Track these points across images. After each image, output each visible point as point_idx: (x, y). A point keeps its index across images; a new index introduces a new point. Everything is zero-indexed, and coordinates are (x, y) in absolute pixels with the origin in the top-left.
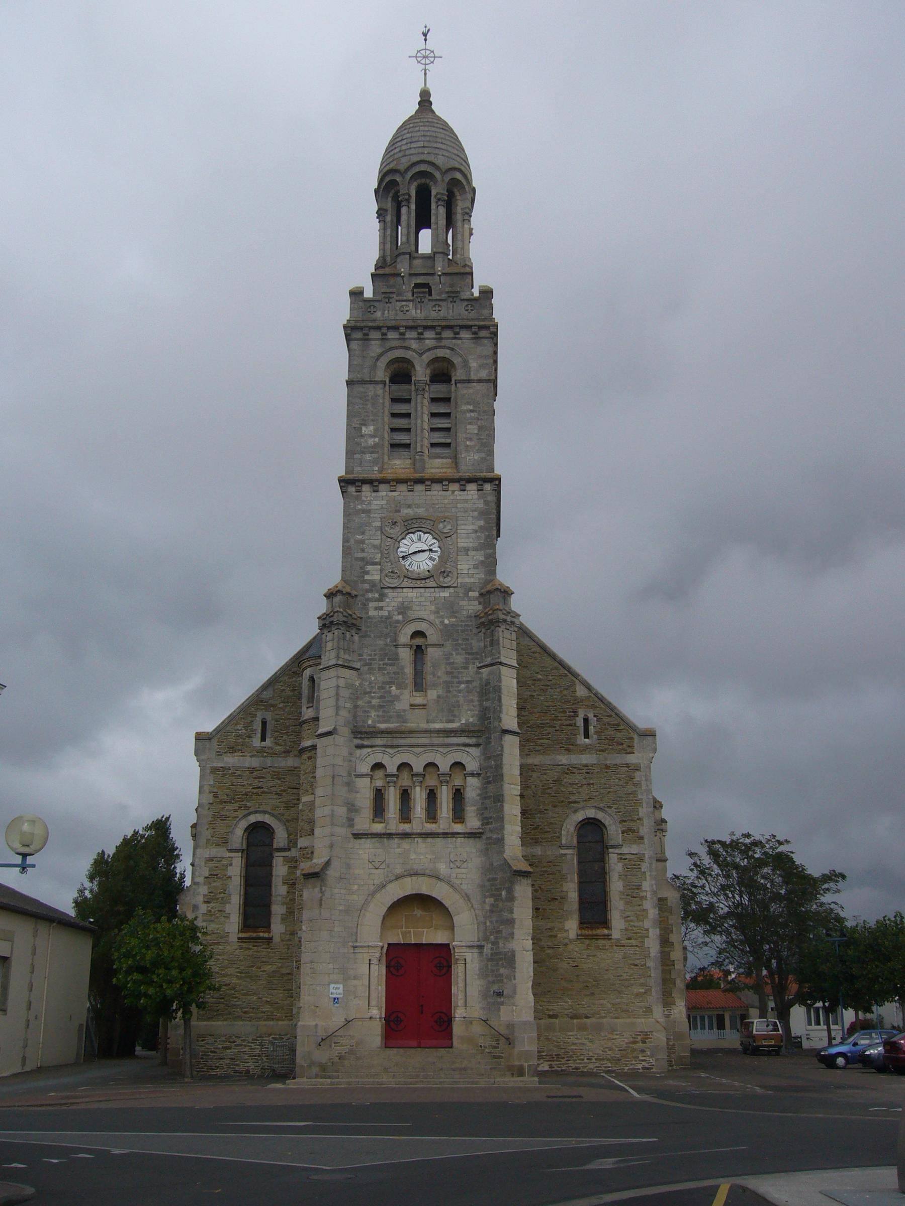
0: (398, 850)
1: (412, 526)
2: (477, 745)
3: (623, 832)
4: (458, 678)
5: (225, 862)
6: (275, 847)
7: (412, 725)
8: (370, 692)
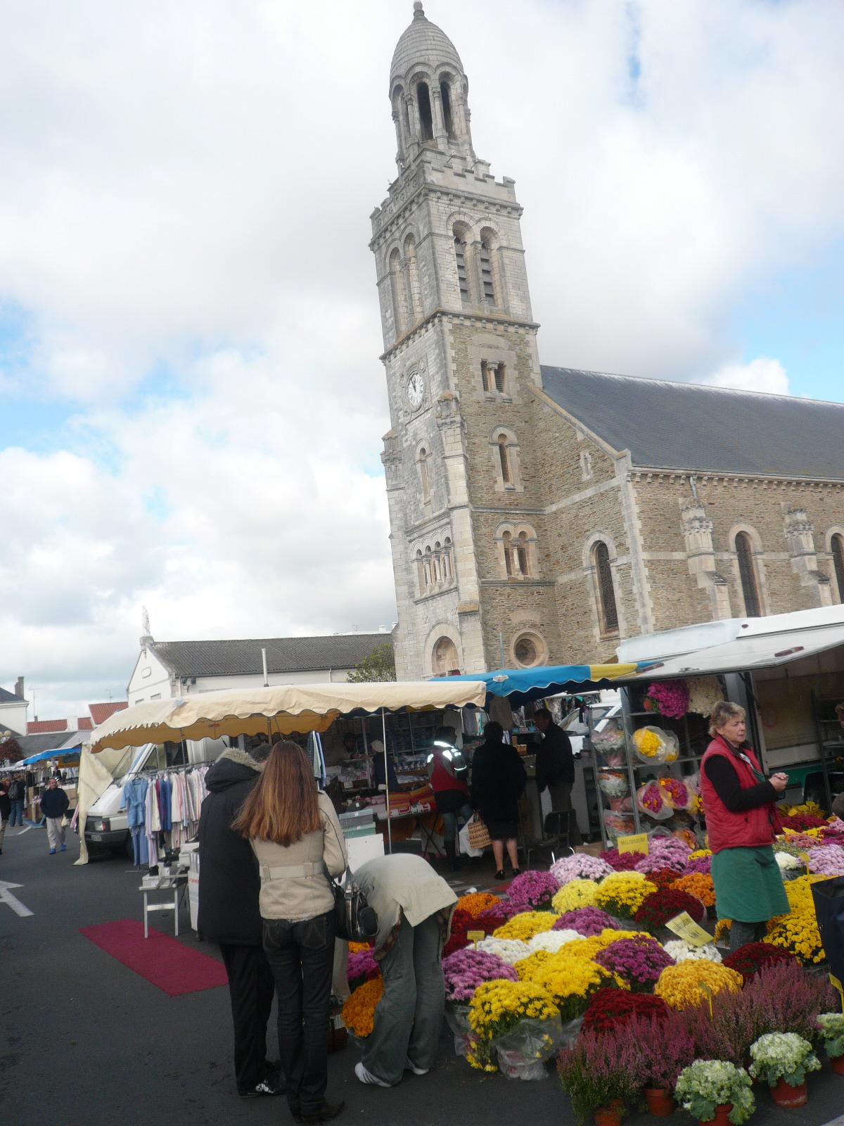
3: (616, 547)
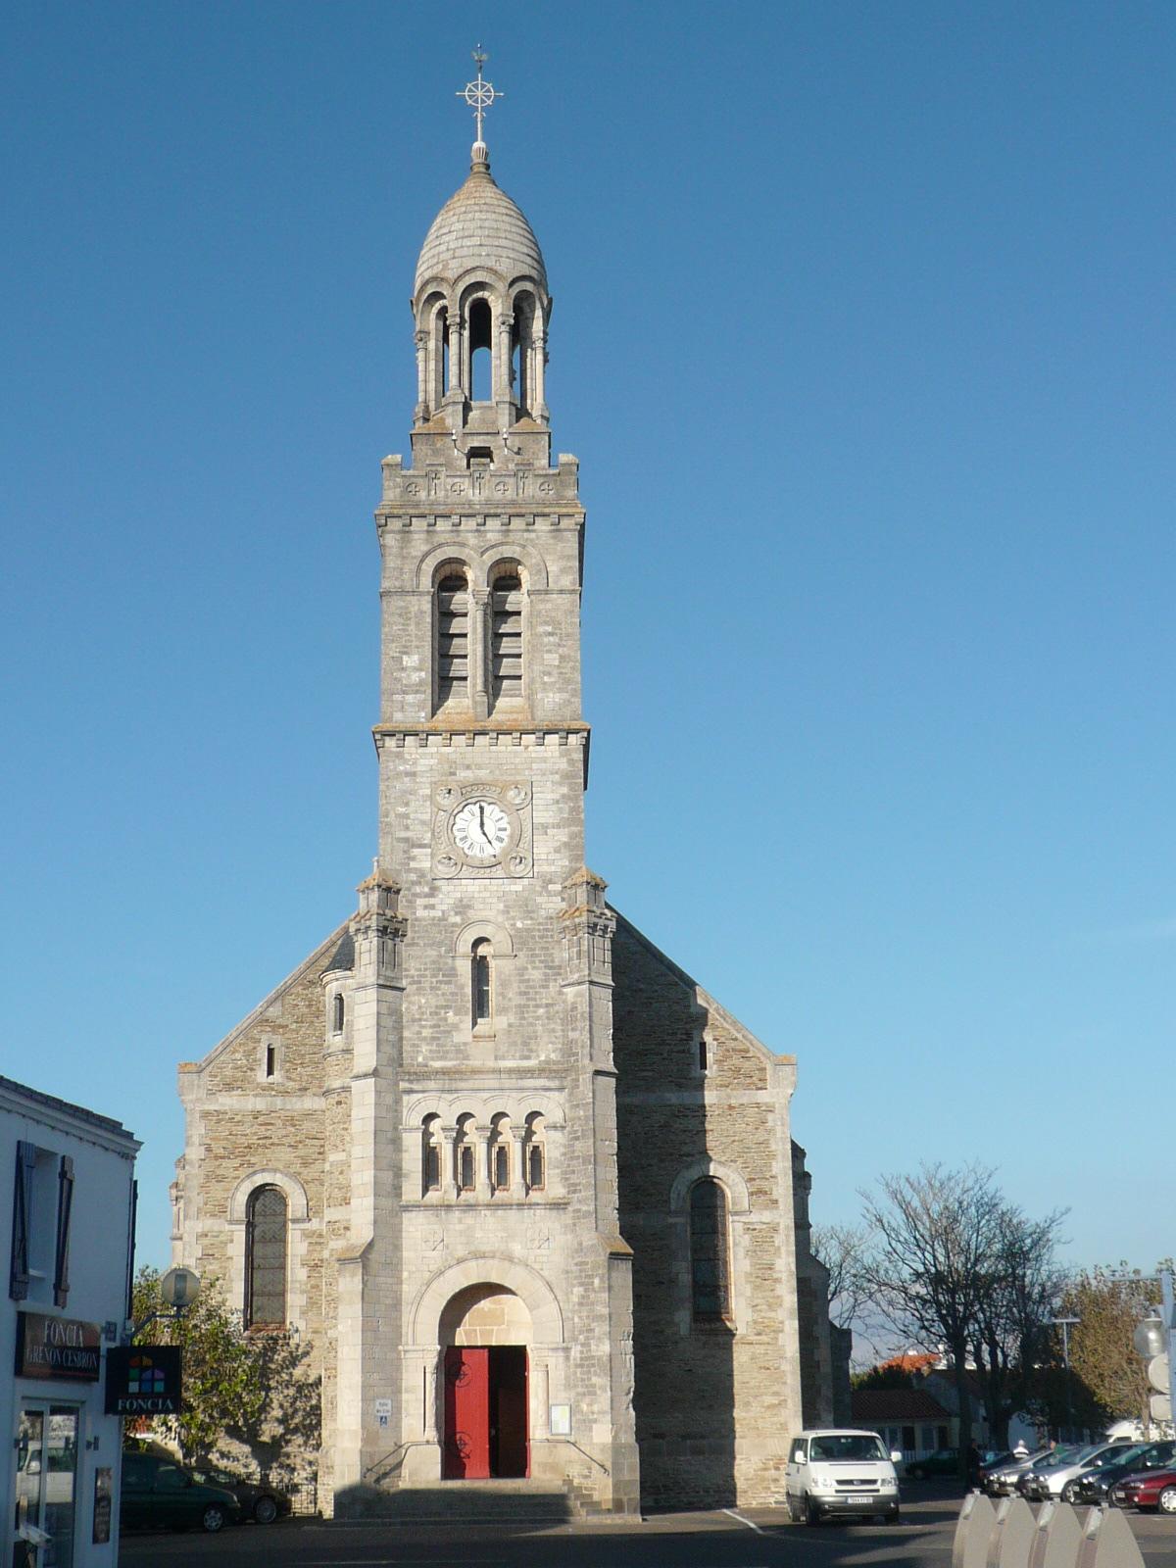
0: (458, 1227)
1: (471, 794)
2: (561, 1089)
3: (751, 1194)
4: (535, 1000)
5: (223, 1238)
6: (290, 1216)
7: (475, 1063)
8: (420, 1020)
